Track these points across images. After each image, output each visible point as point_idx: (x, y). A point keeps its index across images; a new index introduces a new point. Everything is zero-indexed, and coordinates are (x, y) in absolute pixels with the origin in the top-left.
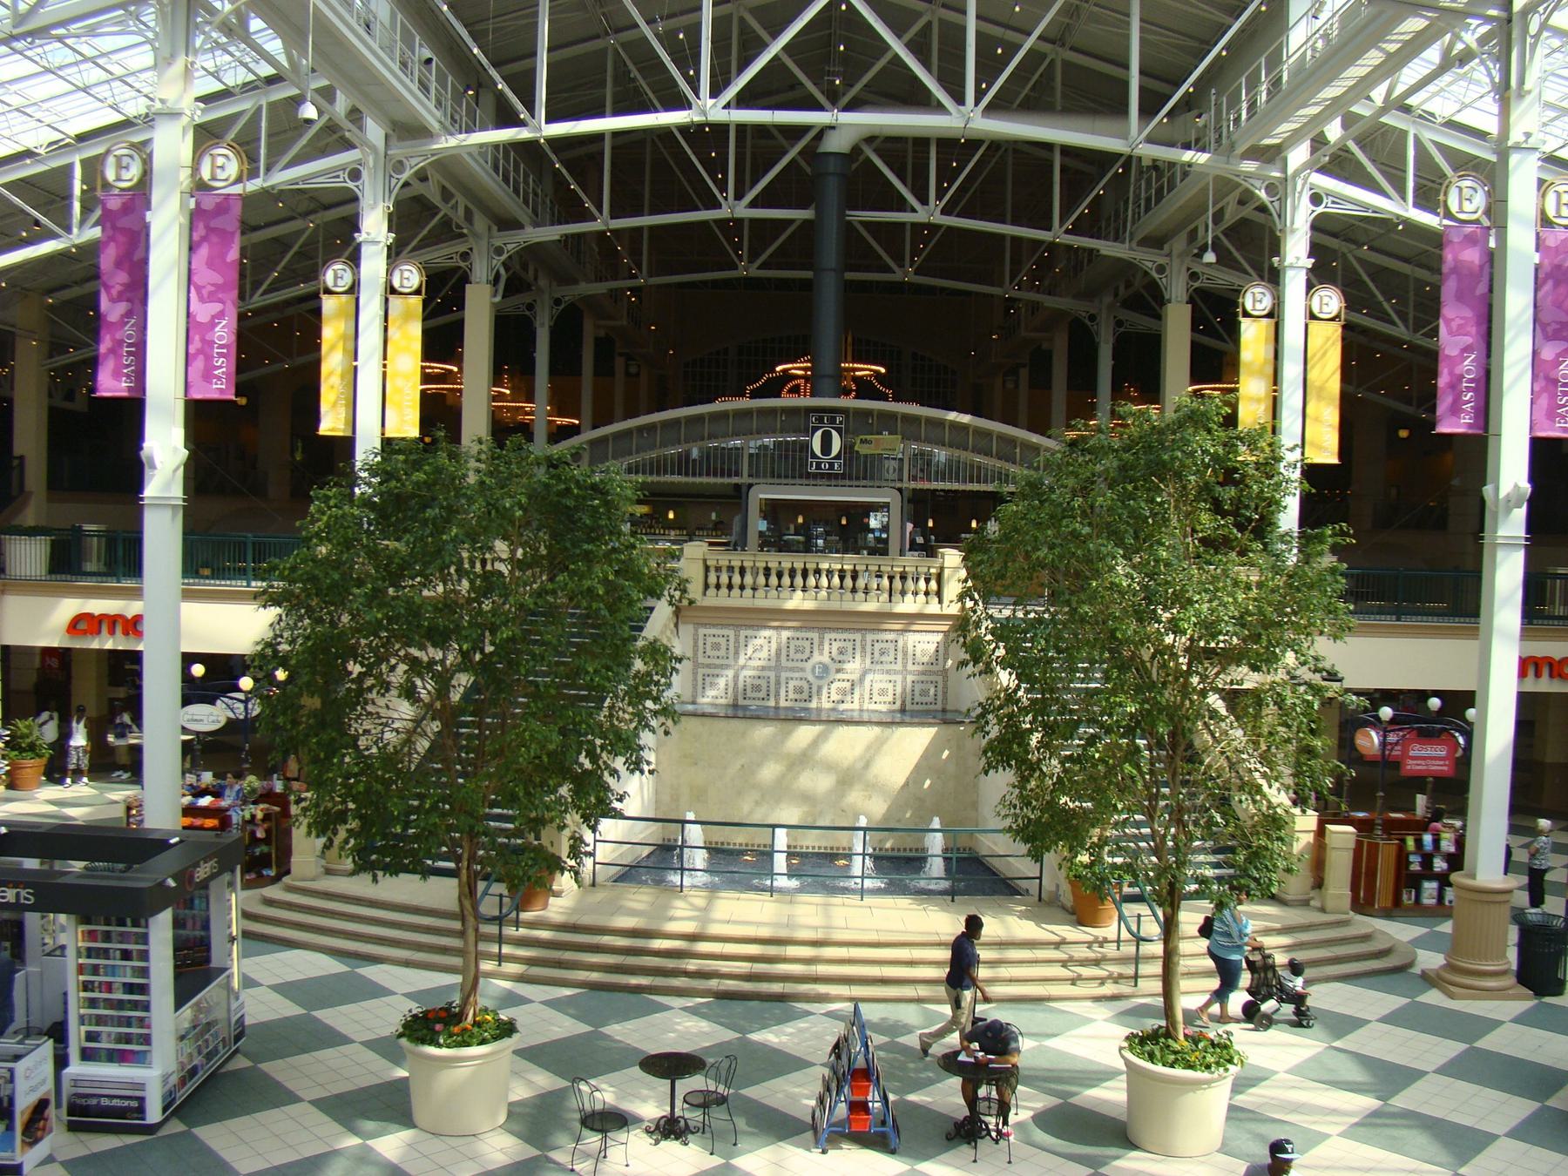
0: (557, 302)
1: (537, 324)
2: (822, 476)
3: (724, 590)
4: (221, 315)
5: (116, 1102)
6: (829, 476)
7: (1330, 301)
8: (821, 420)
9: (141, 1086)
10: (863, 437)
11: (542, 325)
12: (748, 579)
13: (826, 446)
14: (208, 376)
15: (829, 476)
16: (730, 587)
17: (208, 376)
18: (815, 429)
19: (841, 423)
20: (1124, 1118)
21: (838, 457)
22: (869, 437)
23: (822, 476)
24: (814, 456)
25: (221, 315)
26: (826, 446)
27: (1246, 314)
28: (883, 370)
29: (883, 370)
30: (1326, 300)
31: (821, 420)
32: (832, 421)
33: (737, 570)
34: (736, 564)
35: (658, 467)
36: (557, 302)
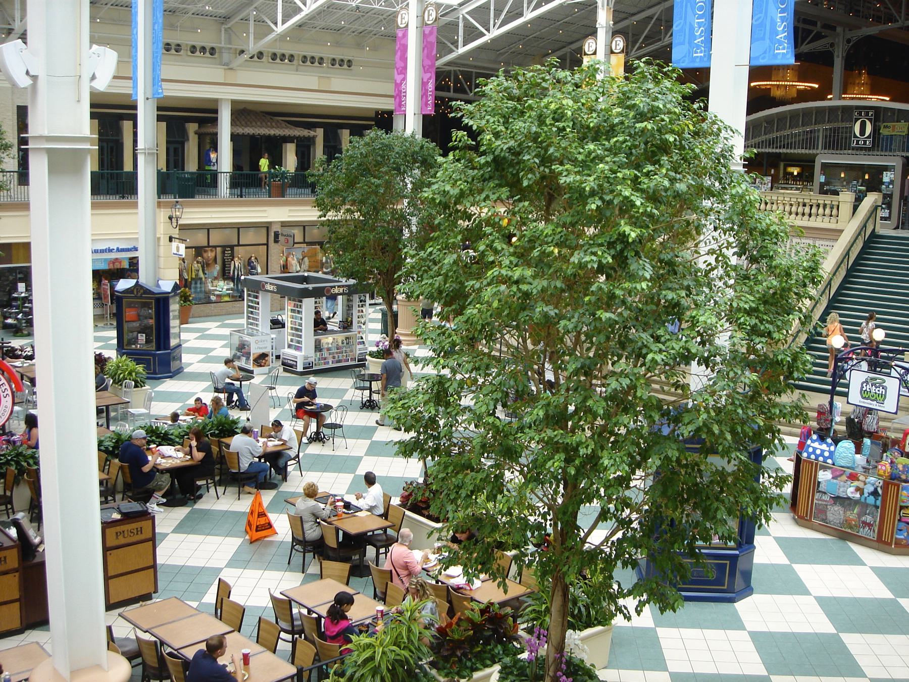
0: (849, 41)
1: (836, 54)
2: (861, 149)
3: (806, 217)
4: (430, 78)
5: (291, 362)
6: (865, 149)
7: (619, 43)
8: (860, 114)
9: (296, 357)
10: (885, 124)
11: (838, 56)
12: (814, 210)
13: (862, 131)
14: (427, 105)
15: (865, 149)
16: (810, 215)
17: (427, 105)
18: (857, 120)
19: (872, 115)
20: (262, 491)
21: (869, 137)
22: (889, 124)
23: (861, 149)
24: (855, 136)
25: (430, 78)
26: (862, 131)
27: (585, 54)
28: (816, 86)
29: (816, 86)
30: (618, 42)
31: (860, 114)
32: (867, 114)
33: (821, 206)
34: (821, 202)
35: (771, 143)
36: (849, 41)
